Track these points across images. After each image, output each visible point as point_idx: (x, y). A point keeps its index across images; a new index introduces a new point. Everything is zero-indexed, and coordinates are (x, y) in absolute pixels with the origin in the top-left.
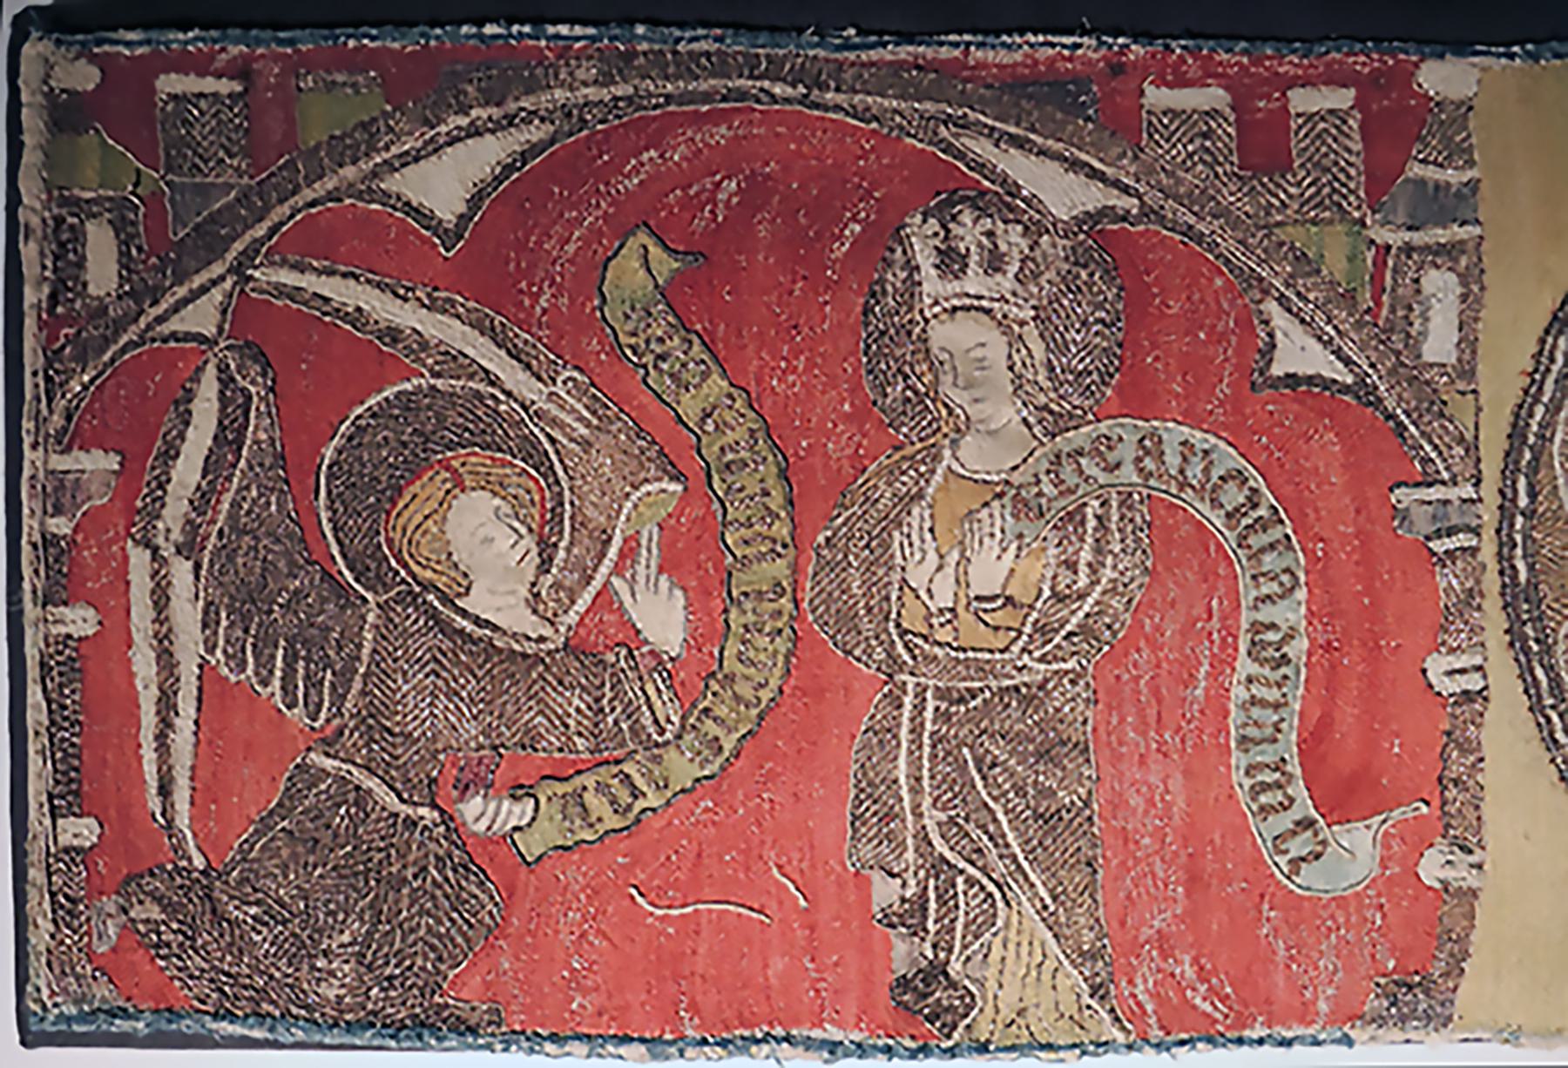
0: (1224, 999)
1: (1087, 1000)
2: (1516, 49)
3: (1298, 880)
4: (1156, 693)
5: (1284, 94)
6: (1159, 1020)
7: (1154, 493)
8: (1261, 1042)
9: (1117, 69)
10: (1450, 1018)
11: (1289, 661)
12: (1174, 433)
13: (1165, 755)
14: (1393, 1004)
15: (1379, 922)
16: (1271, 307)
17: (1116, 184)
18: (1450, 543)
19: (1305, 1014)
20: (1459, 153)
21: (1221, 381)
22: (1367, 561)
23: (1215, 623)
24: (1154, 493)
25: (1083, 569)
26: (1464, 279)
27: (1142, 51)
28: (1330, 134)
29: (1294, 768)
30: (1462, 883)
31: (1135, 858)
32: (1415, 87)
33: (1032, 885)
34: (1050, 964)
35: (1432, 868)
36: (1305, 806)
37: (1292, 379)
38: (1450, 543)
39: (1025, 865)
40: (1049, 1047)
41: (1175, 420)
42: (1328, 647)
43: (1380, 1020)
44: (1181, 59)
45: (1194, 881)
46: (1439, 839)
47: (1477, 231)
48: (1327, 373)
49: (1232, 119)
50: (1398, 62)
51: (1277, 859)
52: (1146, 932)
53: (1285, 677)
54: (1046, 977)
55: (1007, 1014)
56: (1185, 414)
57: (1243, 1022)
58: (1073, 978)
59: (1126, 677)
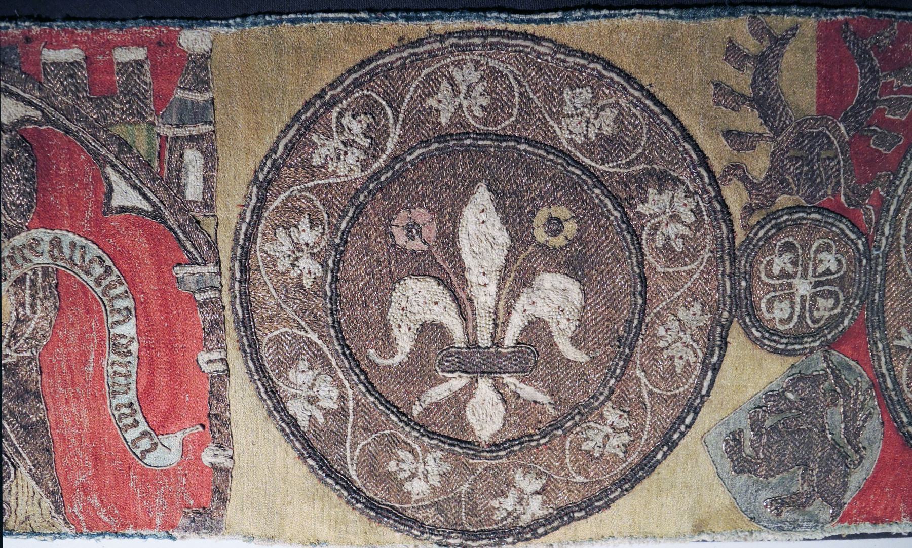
0: (115, 516)
1: (53, 514)
2: (231, 22)
3: (145, 461)
4: (70, 368)
5: (111, 51)
6: (86, 525)
7: (60, 268)
8: (132, 535)
9: (28, 40)
10: (221, 529)
11: (132, 354)
12: (68, 237)
13: (78, 399)
14: (192, 522)
15: (184, 482)
16: (109, 170)
17: (30, 103)
18: (205, 296)
19: (150, 525)
20: (202, 84)
21: (87, 210)
22: (165, 306)
23: (94, 334)
24: (60, 268)
25: (710, 189)
26: (205, 156)
27: (38, 29)
28: (135, 74)
29: (136, 406)
30: (222, 465)
31: (69, 448)
32: (178, 46)
33: (24, 459)
34: (37, 496)
35: (207, 458)
36: (143, 427)
37: (123, 209)
38: (205, 296)
39: (20, 449)
40: (39, 534)
41: (67, 230)
42: (148, 348)
43: (186, 529)
44: (58, 33)
45: (96, 458)
46: (211, 444)
47: (211, 128)
48: (141, 206)
49: (85, 66)
50: (170, 31)
51: (134, 450)
52: (77, 483)
53: (129, 362)
54: (36, 502)
55: (21, 518)
56: (72, 226)
57: (124, 526)
58: (47, 503)
59: (54, 360)
